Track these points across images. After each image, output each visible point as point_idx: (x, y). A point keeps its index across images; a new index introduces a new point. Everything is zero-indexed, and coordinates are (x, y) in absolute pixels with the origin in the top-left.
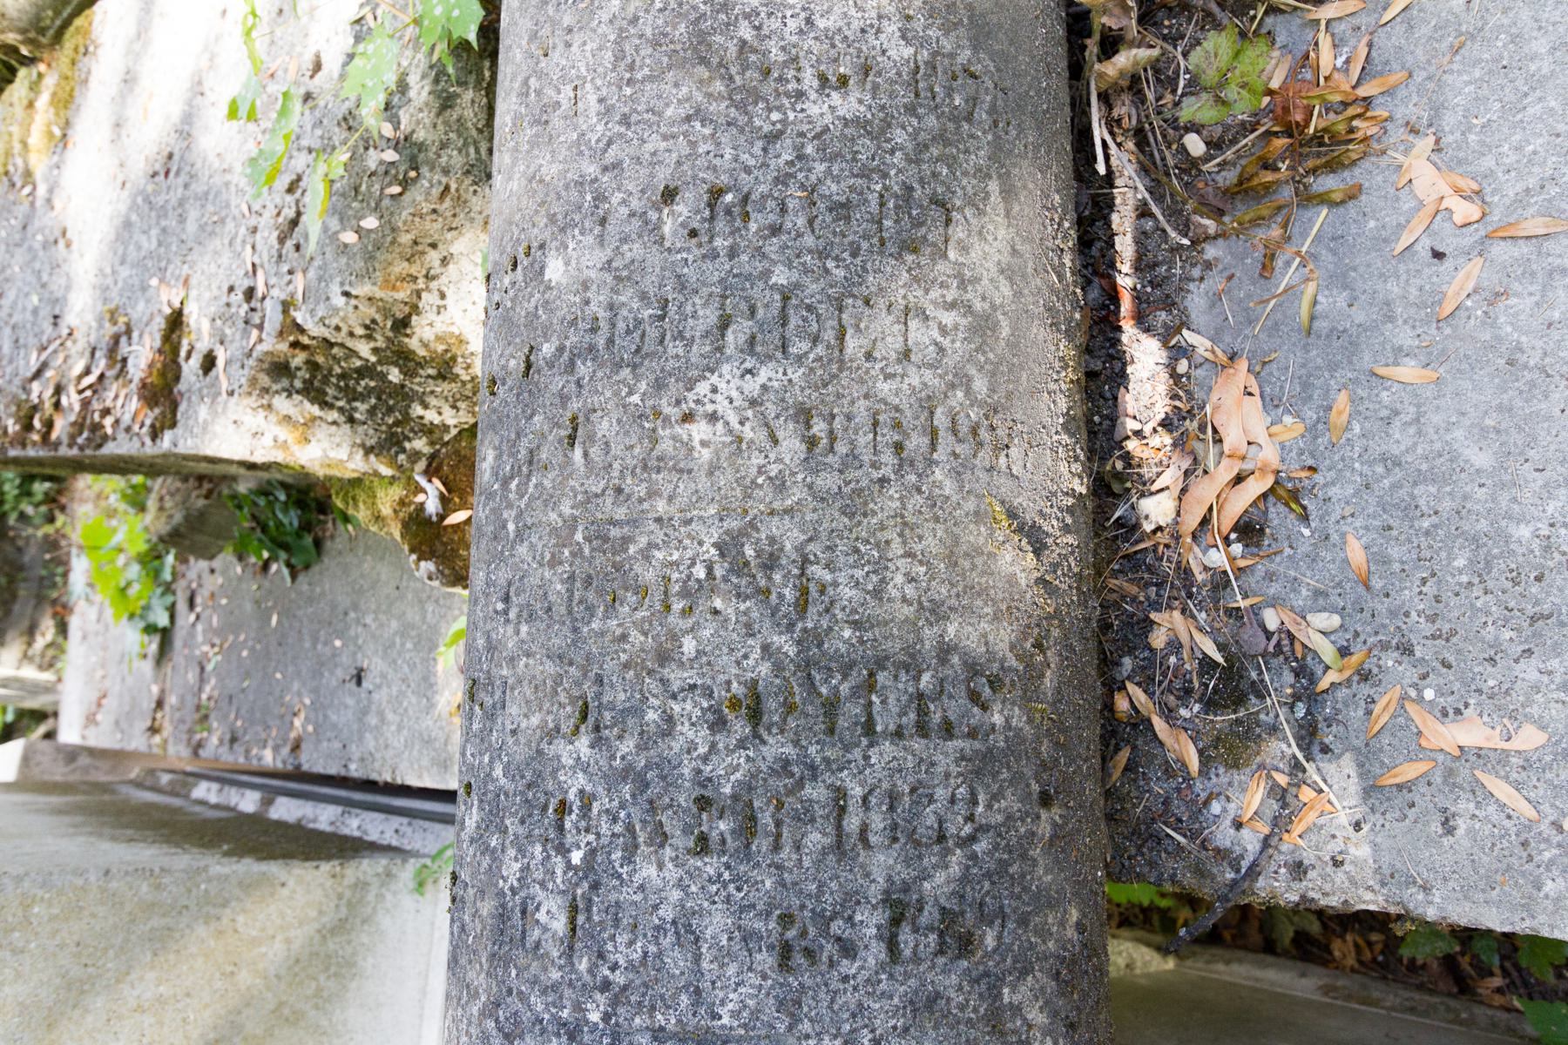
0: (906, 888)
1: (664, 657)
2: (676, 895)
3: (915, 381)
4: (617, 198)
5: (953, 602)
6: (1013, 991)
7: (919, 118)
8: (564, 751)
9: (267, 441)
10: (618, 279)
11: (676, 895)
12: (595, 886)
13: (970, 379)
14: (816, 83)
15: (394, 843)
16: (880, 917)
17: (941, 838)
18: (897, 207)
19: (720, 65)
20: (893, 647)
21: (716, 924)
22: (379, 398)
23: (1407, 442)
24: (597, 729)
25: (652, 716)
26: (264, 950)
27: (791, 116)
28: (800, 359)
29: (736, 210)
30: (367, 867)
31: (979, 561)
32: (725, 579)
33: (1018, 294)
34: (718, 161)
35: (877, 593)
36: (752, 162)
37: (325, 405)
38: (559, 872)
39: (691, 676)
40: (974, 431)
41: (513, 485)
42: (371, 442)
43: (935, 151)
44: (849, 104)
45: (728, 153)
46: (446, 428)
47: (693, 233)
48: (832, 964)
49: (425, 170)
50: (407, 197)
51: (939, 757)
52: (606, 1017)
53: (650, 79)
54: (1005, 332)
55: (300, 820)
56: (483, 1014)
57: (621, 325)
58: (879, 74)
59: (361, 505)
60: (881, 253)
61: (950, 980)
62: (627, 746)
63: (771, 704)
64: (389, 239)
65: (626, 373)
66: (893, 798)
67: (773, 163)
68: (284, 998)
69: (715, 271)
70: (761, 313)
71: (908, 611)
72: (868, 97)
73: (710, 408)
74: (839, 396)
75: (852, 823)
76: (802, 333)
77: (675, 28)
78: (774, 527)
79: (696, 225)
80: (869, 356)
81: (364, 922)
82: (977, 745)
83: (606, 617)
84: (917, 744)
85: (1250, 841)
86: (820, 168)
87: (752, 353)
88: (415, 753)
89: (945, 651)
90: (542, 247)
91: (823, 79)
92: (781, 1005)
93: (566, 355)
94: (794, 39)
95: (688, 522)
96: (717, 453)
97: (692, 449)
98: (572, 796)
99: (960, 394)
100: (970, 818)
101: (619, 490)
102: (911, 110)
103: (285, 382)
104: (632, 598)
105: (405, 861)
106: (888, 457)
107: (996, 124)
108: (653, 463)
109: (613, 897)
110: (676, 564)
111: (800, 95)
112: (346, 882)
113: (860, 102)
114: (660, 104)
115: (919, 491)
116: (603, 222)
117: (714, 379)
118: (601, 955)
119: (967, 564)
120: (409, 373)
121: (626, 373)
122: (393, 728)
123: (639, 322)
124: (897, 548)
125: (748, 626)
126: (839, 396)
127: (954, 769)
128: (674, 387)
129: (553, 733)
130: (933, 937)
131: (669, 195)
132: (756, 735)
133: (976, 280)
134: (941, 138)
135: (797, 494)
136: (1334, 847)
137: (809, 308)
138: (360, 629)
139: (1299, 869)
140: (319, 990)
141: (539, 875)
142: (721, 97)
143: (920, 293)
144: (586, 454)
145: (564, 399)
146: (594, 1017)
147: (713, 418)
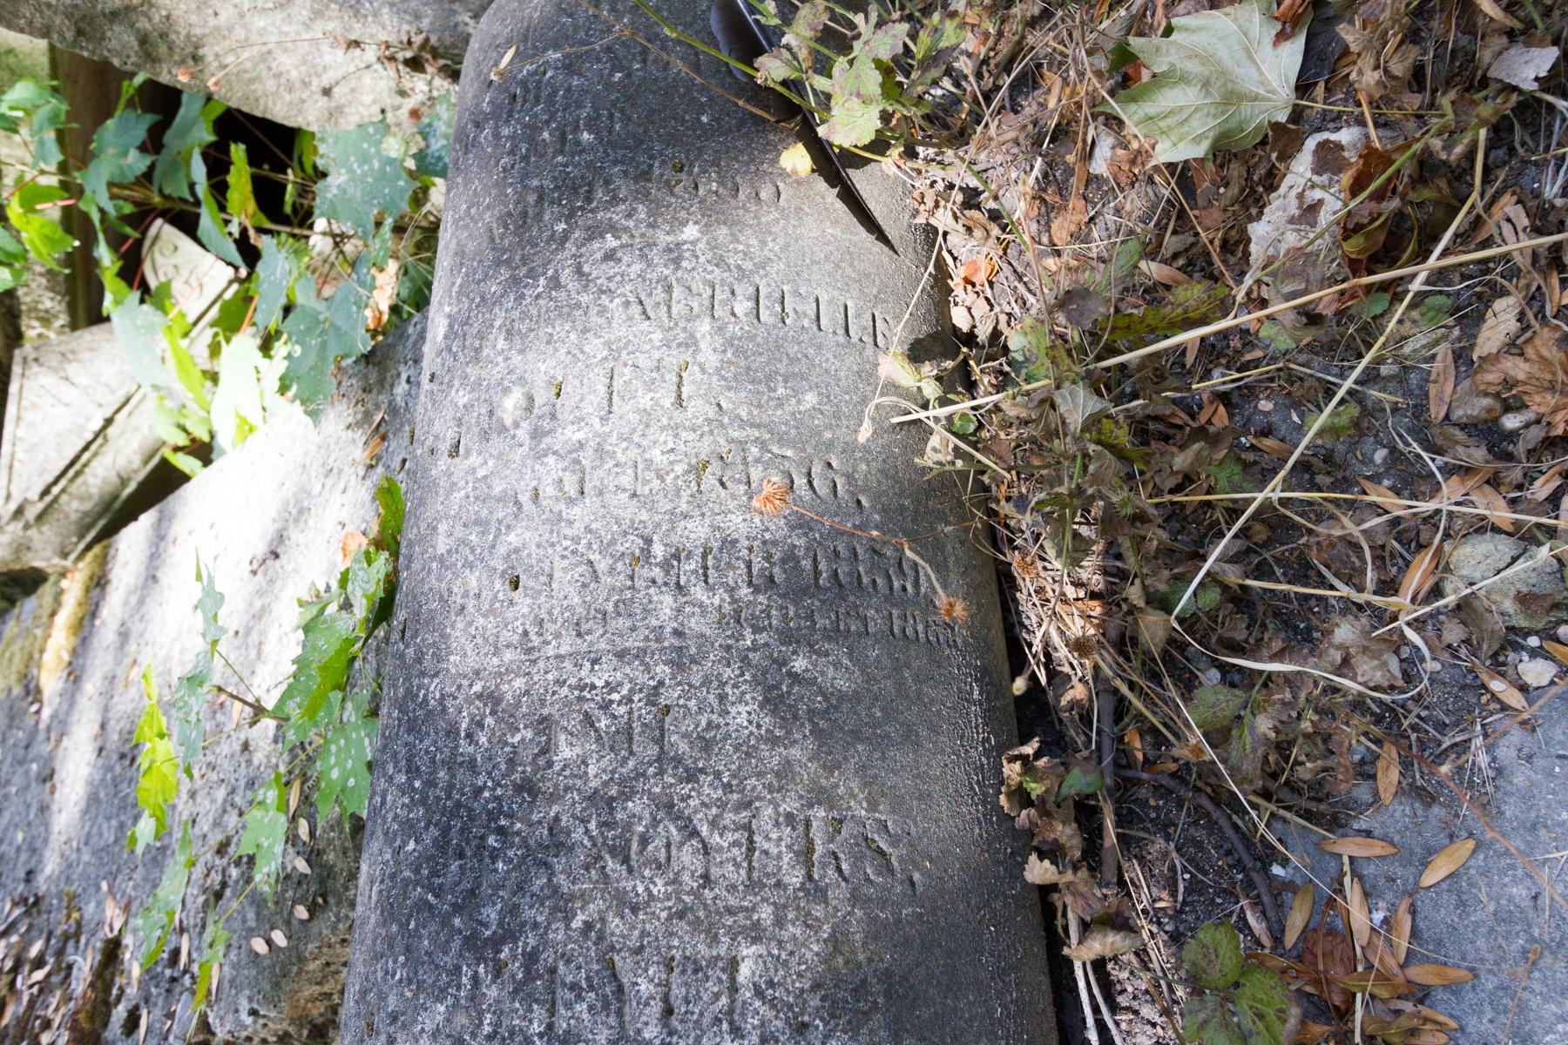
50: (315, 927)
64: (295, 969)
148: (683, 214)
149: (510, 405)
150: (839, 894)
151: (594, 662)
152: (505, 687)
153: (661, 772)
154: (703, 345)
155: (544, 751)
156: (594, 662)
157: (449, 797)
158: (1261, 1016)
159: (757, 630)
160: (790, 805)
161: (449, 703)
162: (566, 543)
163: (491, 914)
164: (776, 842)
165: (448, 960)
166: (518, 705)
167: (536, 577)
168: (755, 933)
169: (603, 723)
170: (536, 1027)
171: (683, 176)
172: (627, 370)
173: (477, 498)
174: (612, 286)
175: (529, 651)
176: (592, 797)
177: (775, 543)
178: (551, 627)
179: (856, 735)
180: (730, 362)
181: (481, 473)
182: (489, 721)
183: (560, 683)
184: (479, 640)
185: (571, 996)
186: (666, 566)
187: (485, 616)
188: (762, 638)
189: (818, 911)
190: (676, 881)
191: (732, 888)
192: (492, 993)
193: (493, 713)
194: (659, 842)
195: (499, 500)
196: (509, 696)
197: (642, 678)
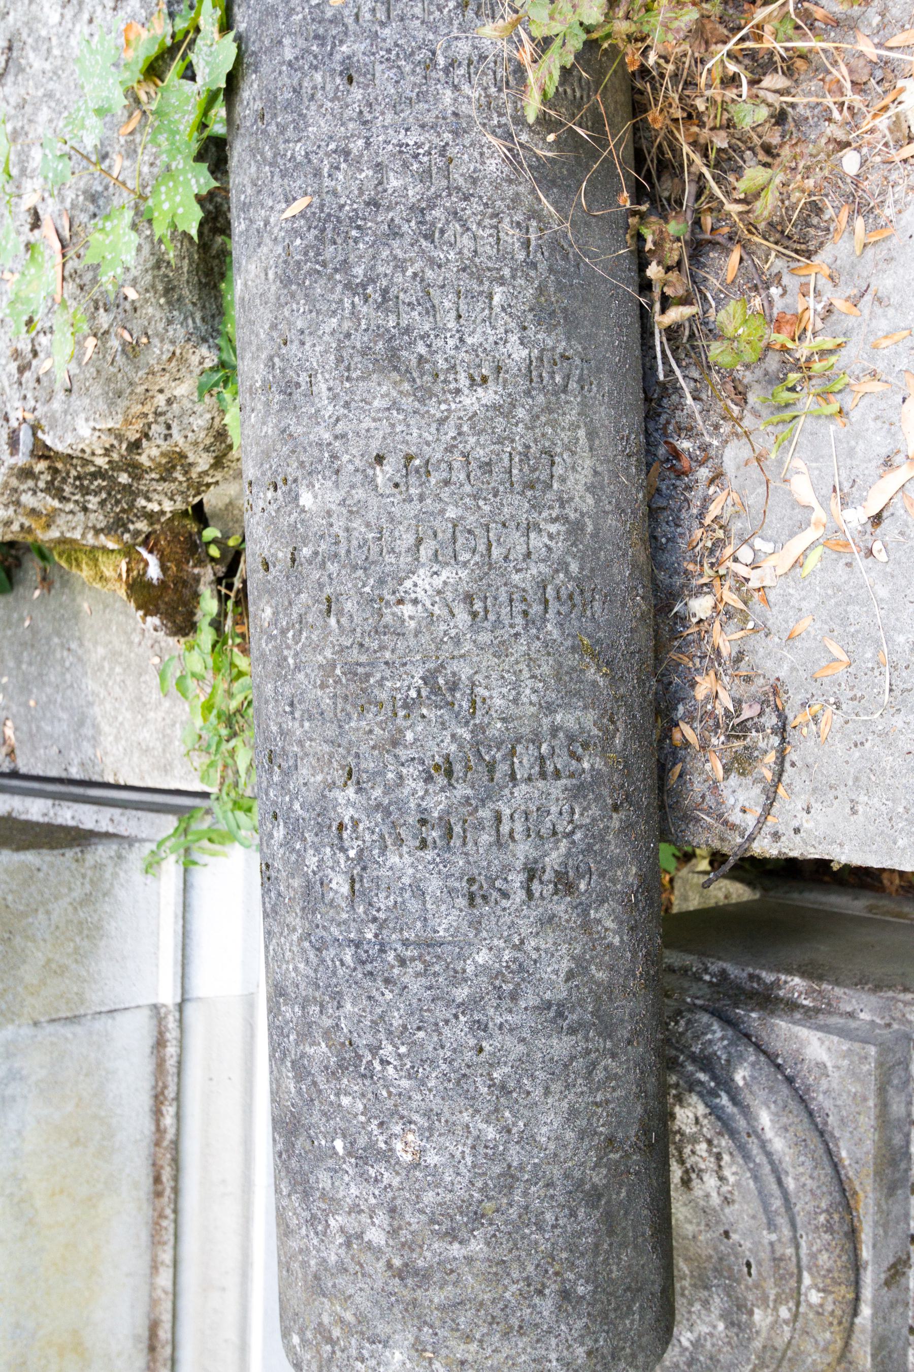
0: (536, 861)
1: (395, 743)
2: (411, 871)
3: (534, 571)
4: (345, 458)
5: (560, 702)
6: (597, 911)
7: (533, 398)
8: (339, 796)
9: (15, 527)
10: (350, 512)
11: (411, 871)
12: (364, 869)
13: (567, 565)
14: (468, 383)
15: (111, 830)
16: (522, 877)
17: (555, 833)
18: (521, 461)
19: (407, 371)
20: (525, 731)
21: (434, 885)
22: (109, 494)
23: (845, 577)
24: (358, 783)
25: (390, 776)
27: (453, 406)
28: (465, 564)
30: (102, 852)
31: (574, 675)
32: (428, 698)
33: (598, 501)
34: (408, 438)
35: (515, 701)
36: (430, 438)
37: (63, 499)
38: (342, 862)
39: (412, 753)
40: (571, 597)
41: (290, 634)
42: (100, 526)
44: (488, 395)
45: (415, 433)
46: (163, 513)
47: (396, 485)
48: (496, 903)
49: (156, 341)
51: (552, 790)
52: (376, 936)
53: (362, 378)
54: (590, 529)
55: (10, 814)
56: (300, 939)
57: (355, 543)
58: (507, 372)
59: (84, 566)
60: (512, 492)
61: (561, 907)
62: (377, 793)
63: (458, 768)
65: (360, 572)
66: (527, 815)
67: (443, 438)
68: (50, 956)
69: (413, 509)
70: (440, 535)
71: (533, 709)
72: (500, 389)
73: (413, 596)
74: (489, 586)
75: (505, 829)
76: (465, 548)
77: (376, 343)
78: (454, 666)
79: (397, 480)
80: (506, 558)
81: (105, 895)
82: (574, 781)
83: (359, 720)
84: (540, 784)
85: (750, 821)
87: (437, 561)
88: (135, 759)
89: (555, 731)
90: (295, 481)
91: (472, 379)
92: (470, 924)
93: (320, 558)
94: (453, 352)
95: (405, 664)
96: (419, 623)
97: (403, 621)
98: (346, 820)
99: (561, 575)
100: (571, 822)
101: (361, 645)
102: (528, 393)
103: (30, 483)
104: (374, 709)
105: (131, 845)
106: (519, 620)
107: (582, 388)
108: (381, 629)
109: (375, 873)
110: (399, 689)
111: (458, 391)
112: (87, 864)
114: (369, 397)
116: (337, 472)
117: (415, 578)
118: (370, 904)
119: (567, 678)
120: (137, 478)
121: (360, 572)
122: (111, 738)
123: (366, 541)
124: (526, 674)
125: (443, 724)
126: (489, 586)
127: (561, 796)
128: (391, 583)
129: (332, 786)
130: (551, 886)
131: (380, 459)
132: (450, 785)
133: (571, 499)
134: (548, 409)
135: (467, 646)
136: (795, 823)
137: (470, 532)
138: (65, 653)
139: (776, 836)
140: (76, 950)
141: (330, 863)
142: (407, 394)
143: (536, 515)
144: (338, 622)
145: (321, 586)
146: (369, 936)
147: (415, 602)
150: (543, 266)
151: (407, 130)
152: (351, 146)
153: (450, 195)
155: (380, 183)
156: (407, 130)
157: (322, 211)
159: (500, 115)
160: (518, 217)
161: (313, 157)
163: (359, 271)
164: (511, 236)
165: (335, 297)
166: (362, 156)
168: (502, 281)
170: (391, 324)
173: (313, 20)
175: (365, 123)
178: (378, 108)
182: (343, 166)
183: (387, 142)
184: (328, 117)
185: (407, 309)
186: (446, 71)
187: (332, 101)
189: (532, 273)
190: (460, 253)
191: (489, 258)
192: (365, 309)
193: (345, 161)
195: (331, 22)
196: (355, 151)
197: (436, 141)
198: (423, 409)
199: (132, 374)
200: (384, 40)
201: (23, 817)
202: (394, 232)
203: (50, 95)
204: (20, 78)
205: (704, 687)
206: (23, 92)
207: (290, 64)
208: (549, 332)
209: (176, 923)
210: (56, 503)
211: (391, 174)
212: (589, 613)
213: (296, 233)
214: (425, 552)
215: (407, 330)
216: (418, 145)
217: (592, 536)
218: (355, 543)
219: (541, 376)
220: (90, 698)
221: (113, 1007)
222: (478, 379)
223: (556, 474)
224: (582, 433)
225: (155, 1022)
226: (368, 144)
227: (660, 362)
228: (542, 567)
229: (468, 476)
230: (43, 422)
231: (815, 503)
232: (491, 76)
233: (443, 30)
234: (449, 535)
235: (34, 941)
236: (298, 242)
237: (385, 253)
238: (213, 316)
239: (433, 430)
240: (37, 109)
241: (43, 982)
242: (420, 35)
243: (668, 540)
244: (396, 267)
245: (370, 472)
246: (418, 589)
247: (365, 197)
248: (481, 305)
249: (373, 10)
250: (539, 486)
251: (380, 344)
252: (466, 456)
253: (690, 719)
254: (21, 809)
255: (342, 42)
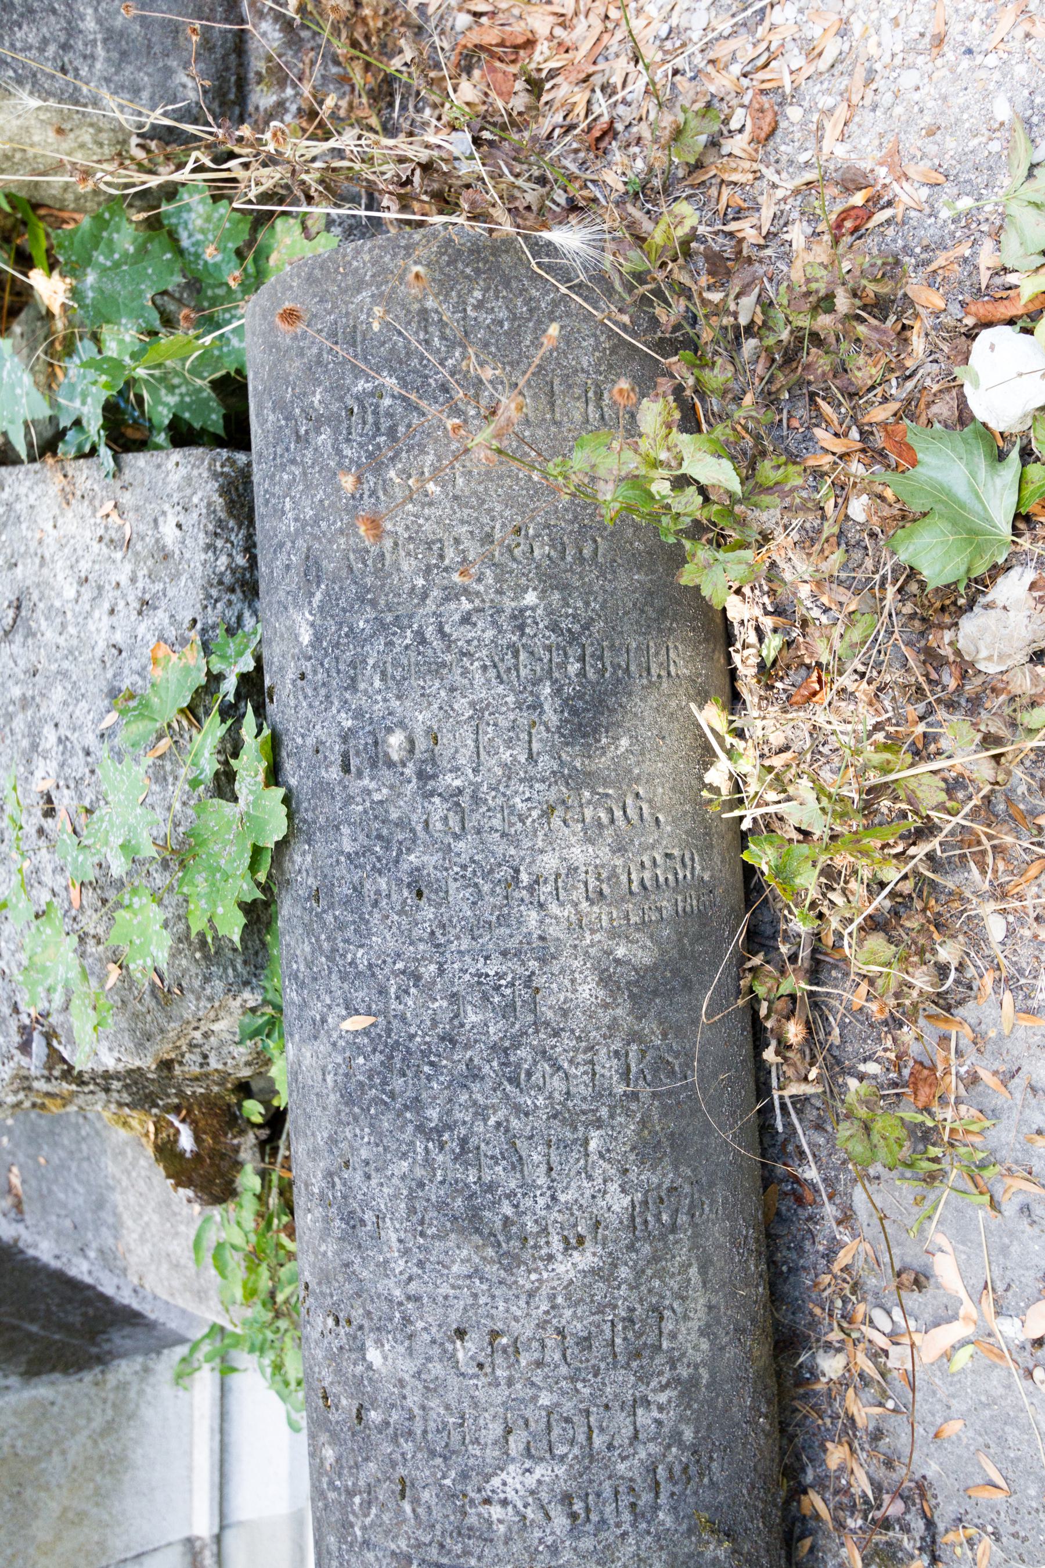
4: (420, 1325)
7: (637, 1251)
13: (680, 1434)
14: (561, 1247)
18: (624, 1328)
26: (43, 1465)
27: (545, 1275)
28: (562, 1458)
29: (510, 1350)
34: (494, 1311)
36: (519, 1313)
43: (649, 1272)
44: (585, 1259)
45: (502, 1305)
55: (16, 1240)
60: (615, 1368)
67: (534, 1313)
68: (66, 1503)
70: (532, 1424)
72: (599, 1249)
73: (502, 1496)
74: (591, 1481)
77: (454, 1199)
79: (481, 1359)
86: (568, 1313)
91: (566, 1240)
93: (391, 1431)
96: (510, 1529)
97: (491, 1524)
101: (442, 1546)
102: (631, 1248)
106: (627, 1516)
108: (464, 1531)
111: (550, 1257)
112: (109, 1386)
113: (594, 1254)
114: (447, 1261)
115: (649, 1533)
116: (410, 1337)
117: (504, 1475)
121: (439, 1461)
122: (135, 1236)
123: (445, 1424)
126: (591, 1481)
128: (476, 1479)
131: (461, 1333)
134: (655, 1259)
137: (567, 1420)
142: (492, 1262)
145: (394, 1464)
147: (504, 1503)
148: (523, 581)
149: (396, 741)
151: (487, 958)
152: (422, 970)
153: (537, 1032)
154: (546, 707)
156: (487, 958)
157: (389, 1036)
158: (885, 1138)
159: (593, 932)
160: (617, 1045)
162: (456, 869)
163: (433, 1113)
164: (608, 1068)
166: (434, 983)
167: (436, 892)
168: (599, 1124)
169: (496, 999)
170: (472, 1179)
171: (521, 540)
172: (490, 729)
173: (376, 817)
174: (472, 649)
175: (438, 946)
176: (493, 1047)
177: (603, 866)
179: (655, 993)
180: (567, 721)
181: (377, 797)
182: (413, 990)
187: (399, 913)
188: (597, 937)
189: (634, 1106)
190: (550, 1097)
192: (440, 1158)
193: (415, 986)
194: (539, 1075)
195: (397, 825)
196: (426, 976)
197: (520, 970)
198: (510, 1280)
199: (163, 1022)
200: (459, 855)
201: (31, 1252)
202: (474, 1074)
203: (65, 674)
204: (30, 641)
205: (836, 1455)
206: (33, 658)
207: (348, 856)
208: (653, 1168)
209: (212, 1439)
210: (74, 1087)
211: (469, 1008)
212: (706, 1480)
213: (360, 1050)
214: (516, 1445)
215: (491, 1188)
216: (500, 976)
217: (707, 1387)
218: (432, 1426)
219: (646, 1222)
220: (111, 1182)
221: (140, 1550)
222: (573, 1241)
223: (666, 1331)
224: (693, 1271)
225: (189, 1558)
226: (441, 971)
227: (778, 1111)
228: (652, 1448)
229: (564, 1356)
230: (59, 1030)
231: (963, 1294)
232: (582, 889)
233: (527, 843)
234: (543, 1425)
235: (48, 1489)
236: (361, 1060)
237: (464, 1098)
238: (256, 953)
239: (522, 1303)
240: (50, 685)
241: (58, 1538)
242: (499, 851)
243: (790, 1269)
244: (476, 1114)
245: (449, 1347)
246: (508, 1489)
247: (439, 1030)
248: (575, 1155)
249: (445, 819)
250: (647, 1353)
251: (459, 1202)
252: (560, 1332)
253: (821, 1484)
254: (30, 1240)
255: (409, 850)
